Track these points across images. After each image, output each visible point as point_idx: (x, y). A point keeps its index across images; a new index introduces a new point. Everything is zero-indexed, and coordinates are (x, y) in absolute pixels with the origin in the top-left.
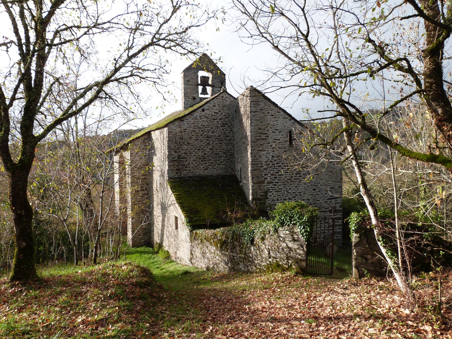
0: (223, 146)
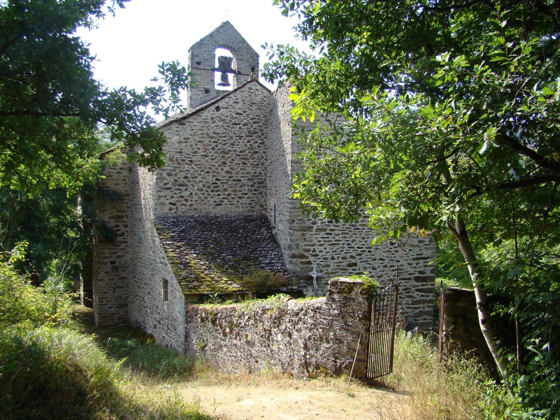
0: (248, 168)
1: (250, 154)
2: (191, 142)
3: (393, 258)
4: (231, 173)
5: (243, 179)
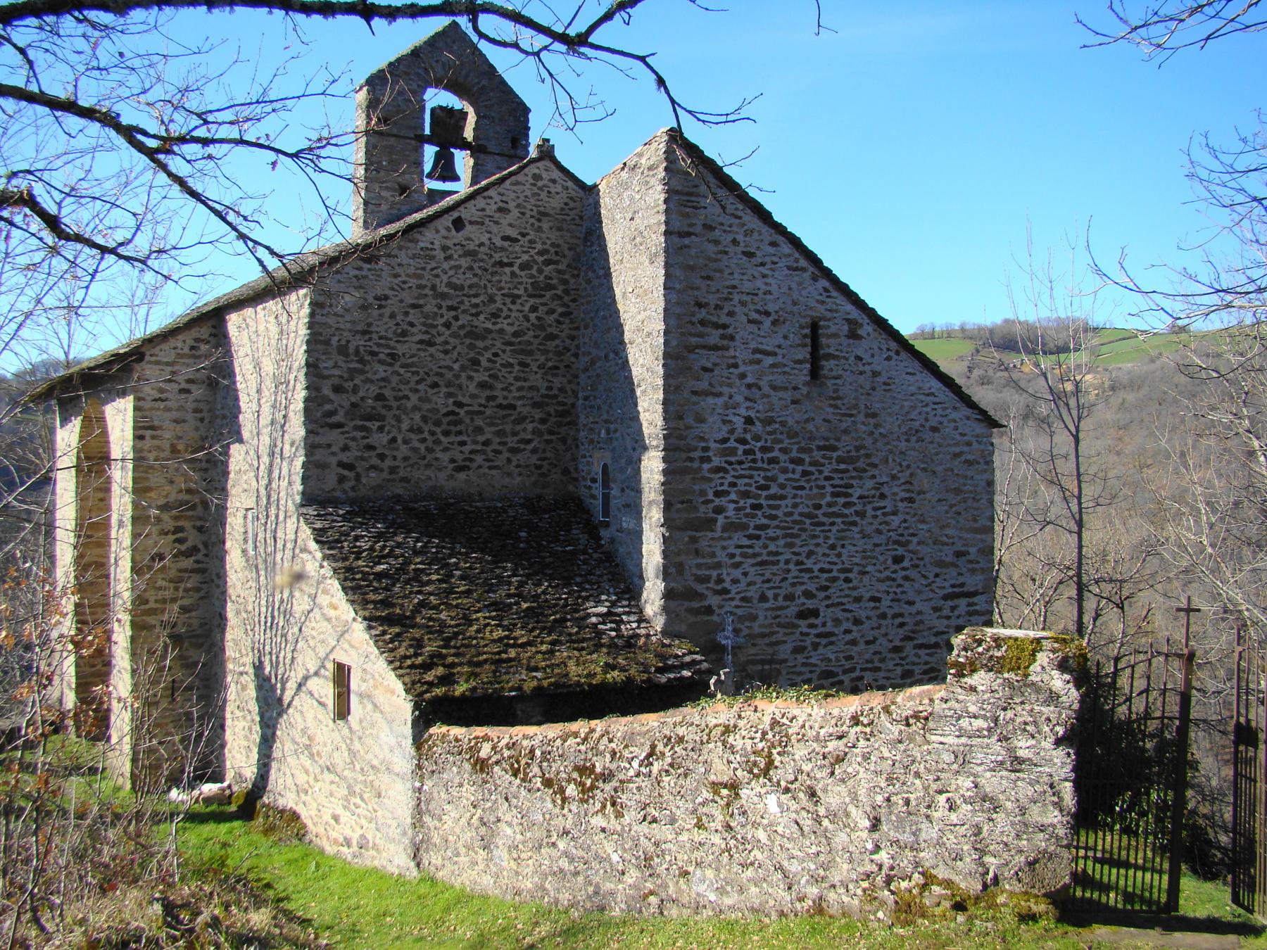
0: (532, 377)
1: (538, 341)
2: (392, 305)
3: (899, 596)
4: (491, 387)
5: (520, 403)
